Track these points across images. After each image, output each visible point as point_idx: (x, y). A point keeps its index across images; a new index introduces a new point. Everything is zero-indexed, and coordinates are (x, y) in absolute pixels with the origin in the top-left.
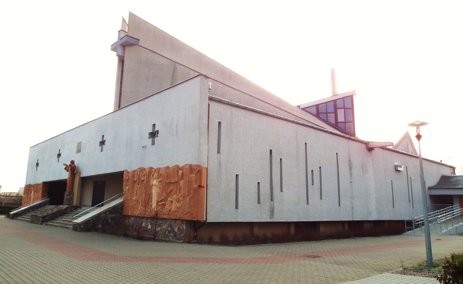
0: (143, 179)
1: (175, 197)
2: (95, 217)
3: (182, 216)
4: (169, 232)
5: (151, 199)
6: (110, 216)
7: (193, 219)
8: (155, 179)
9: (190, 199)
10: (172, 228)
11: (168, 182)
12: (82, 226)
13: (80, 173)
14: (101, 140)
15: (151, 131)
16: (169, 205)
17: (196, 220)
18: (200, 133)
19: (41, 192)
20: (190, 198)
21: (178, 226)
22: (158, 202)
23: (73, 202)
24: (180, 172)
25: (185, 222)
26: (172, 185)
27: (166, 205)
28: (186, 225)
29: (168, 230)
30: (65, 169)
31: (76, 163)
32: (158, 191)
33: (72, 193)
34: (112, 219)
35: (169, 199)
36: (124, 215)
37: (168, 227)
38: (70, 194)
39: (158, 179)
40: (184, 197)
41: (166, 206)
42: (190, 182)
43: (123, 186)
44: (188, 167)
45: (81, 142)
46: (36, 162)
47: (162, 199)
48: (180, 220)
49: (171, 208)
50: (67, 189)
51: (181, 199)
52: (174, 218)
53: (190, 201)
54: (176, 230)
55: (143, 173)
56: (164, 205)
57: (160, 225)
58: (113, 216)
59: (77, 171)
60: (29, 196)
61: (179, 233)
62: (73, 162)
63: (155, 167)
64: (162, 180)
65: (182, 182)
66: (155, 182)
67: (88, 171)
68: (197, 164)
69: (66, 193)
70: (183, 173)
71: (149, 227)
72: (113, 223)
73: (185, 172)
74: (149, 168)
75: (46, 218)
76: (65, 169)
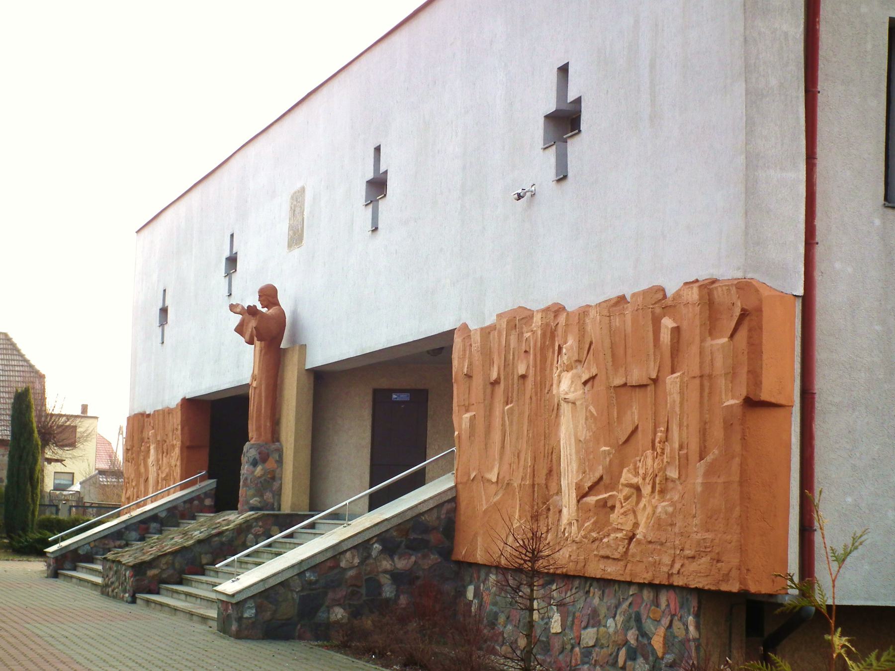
0: (521, 370)
1: (649, 461)
2: (313, 568)
3: (677, 566)
4: (632, 655)
5: (555, 477)
6: (386, 564)
7: (724, 587)
8: (568, 368)
9: (707, 474)
10: (643, 633)
11: (618, 381)
12: (249, 613)
13: (303, 347)
14: (370, 175)
15: (552, 107)
16: (627, 506)
17: (735, 588)
18: (753, 97)
19: (177, 451)
20: (710, 471)
21: (665, 621)
22: (581, 497)
23: (278, 494)
24: (668, 323)
25: (694, 603)
26: (638, 393)
27: (613, 508)
28: (697, 616)
29: (626, 642)
30: (240, 330)
31: (285, 302)
32: (584, 434)
33: (271, 452)
34: (396, 577)
35: (627, 476)
36: (460, 563)
37: (626, 628)
38: (263, 458)
39: (579, 369)
40: (684, 464)
41: (613, 517)
42: (705, 379)
43: (452, 414)
44: (694, 295)
45: (303, 190)
46: (160, 305)
47: (597, 475)
48: (671, 587)
49: (636, 525)
50: (252, 433)
51: (673, 473)
52: (645, 577)
53: (706, 486)
54: (657, 643)
55: (521, 334)
56: (606, 507)
57: (594, 619)
58: (401, 564)
59: (294, 339)
60: (142, 470)
61: (669, 658)
62: (269, 295)
63: (571, 306)
64: (594, 371)
65: (672, 381)
66: (566, 385)
67: (331, 341)
68: (739, 275)
69: (249, 452)
70: (676, 331)
71: (556, 626)
72: (403, 600)
73: (685, 325)
74: (547, 310)
75: (151, 572)
76: (240, 330)
